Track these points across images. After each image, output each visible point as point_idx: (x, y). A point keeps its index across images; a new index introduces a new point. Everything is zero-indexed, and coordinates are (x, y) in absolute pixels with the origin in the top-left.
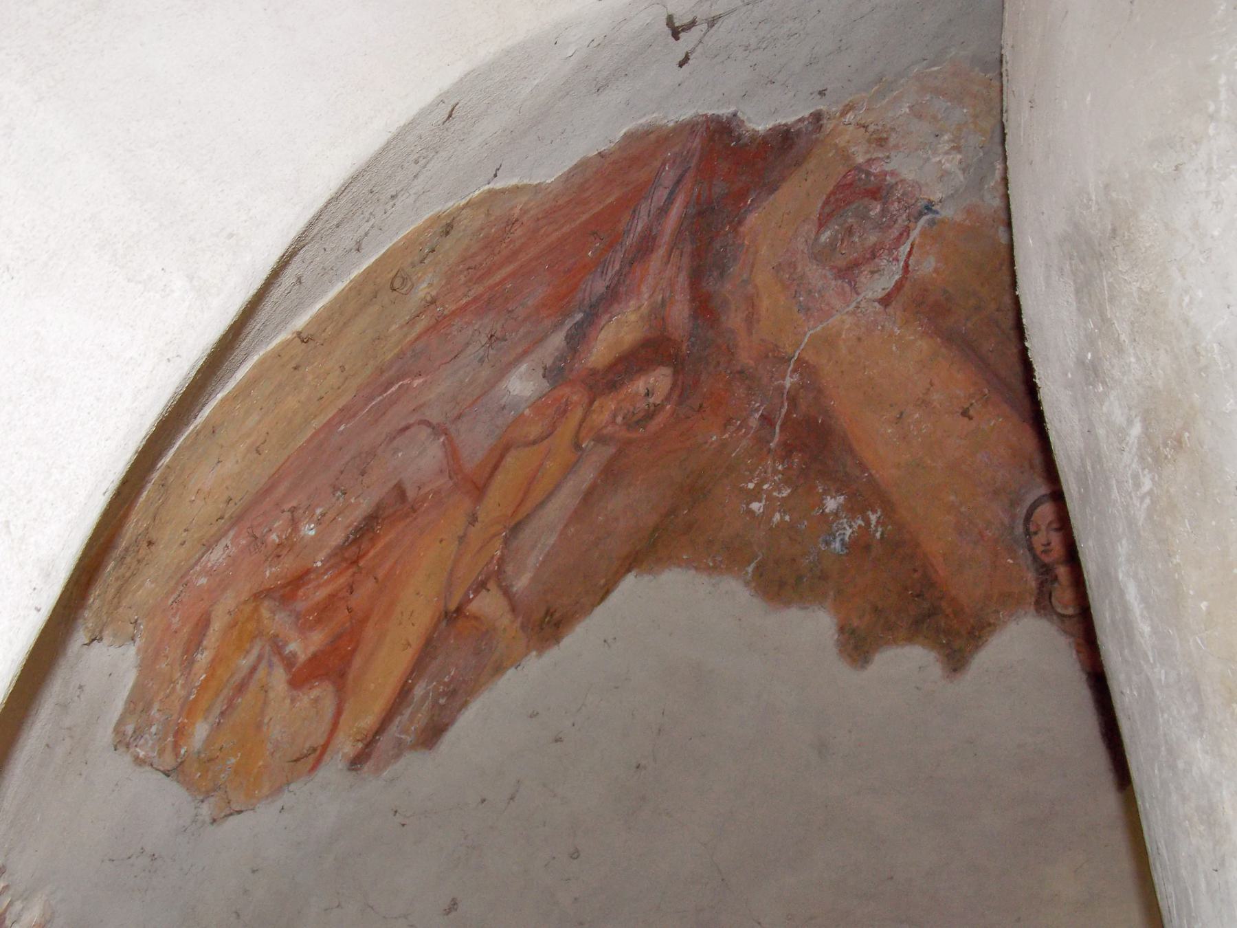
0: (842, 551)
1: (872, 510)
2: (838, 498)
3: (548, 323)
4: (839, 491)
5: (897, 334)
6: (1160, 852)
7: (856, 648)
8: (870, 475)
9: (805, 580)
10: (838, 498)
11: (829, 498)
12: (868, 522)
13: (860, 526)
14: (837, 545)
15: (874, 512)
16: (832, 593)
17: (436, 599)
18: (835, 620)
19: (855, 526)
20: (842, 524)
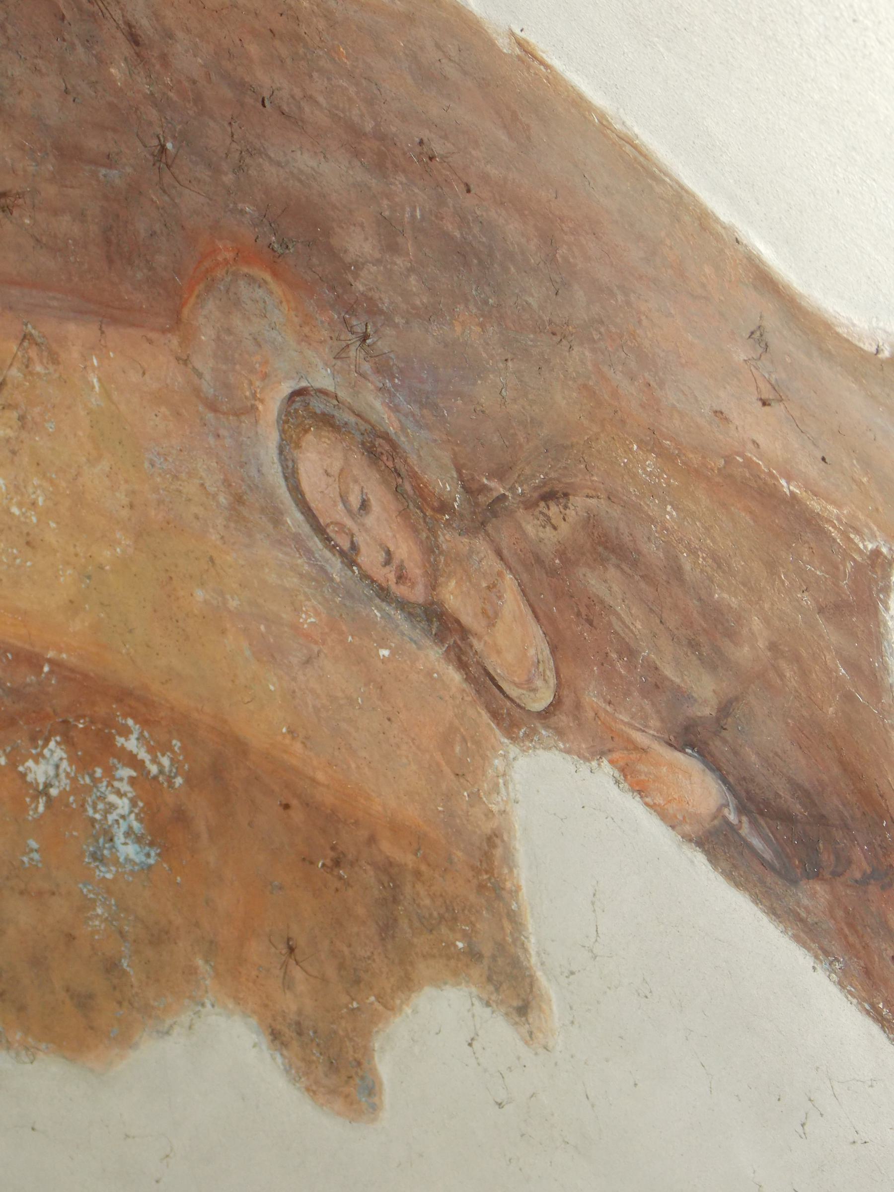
0: (148, 855)
1: (121, 735)
2: (46, 752)
3: (381, 462)
4: (38, 738)
5: (336, 599)
6: (718, 773)
7: (333, 1067)
8: (50, 661)
9: (125, 963)
10: (46, 752)
11: (30, 763)
12: (133, 761)
13: (132, 781)
14: (129, 850)
15: (126, 732)
16: (200, 962)
17: (323, 339)
18: (253, 1021)
19: (125, 787)
20: (102, 798)
